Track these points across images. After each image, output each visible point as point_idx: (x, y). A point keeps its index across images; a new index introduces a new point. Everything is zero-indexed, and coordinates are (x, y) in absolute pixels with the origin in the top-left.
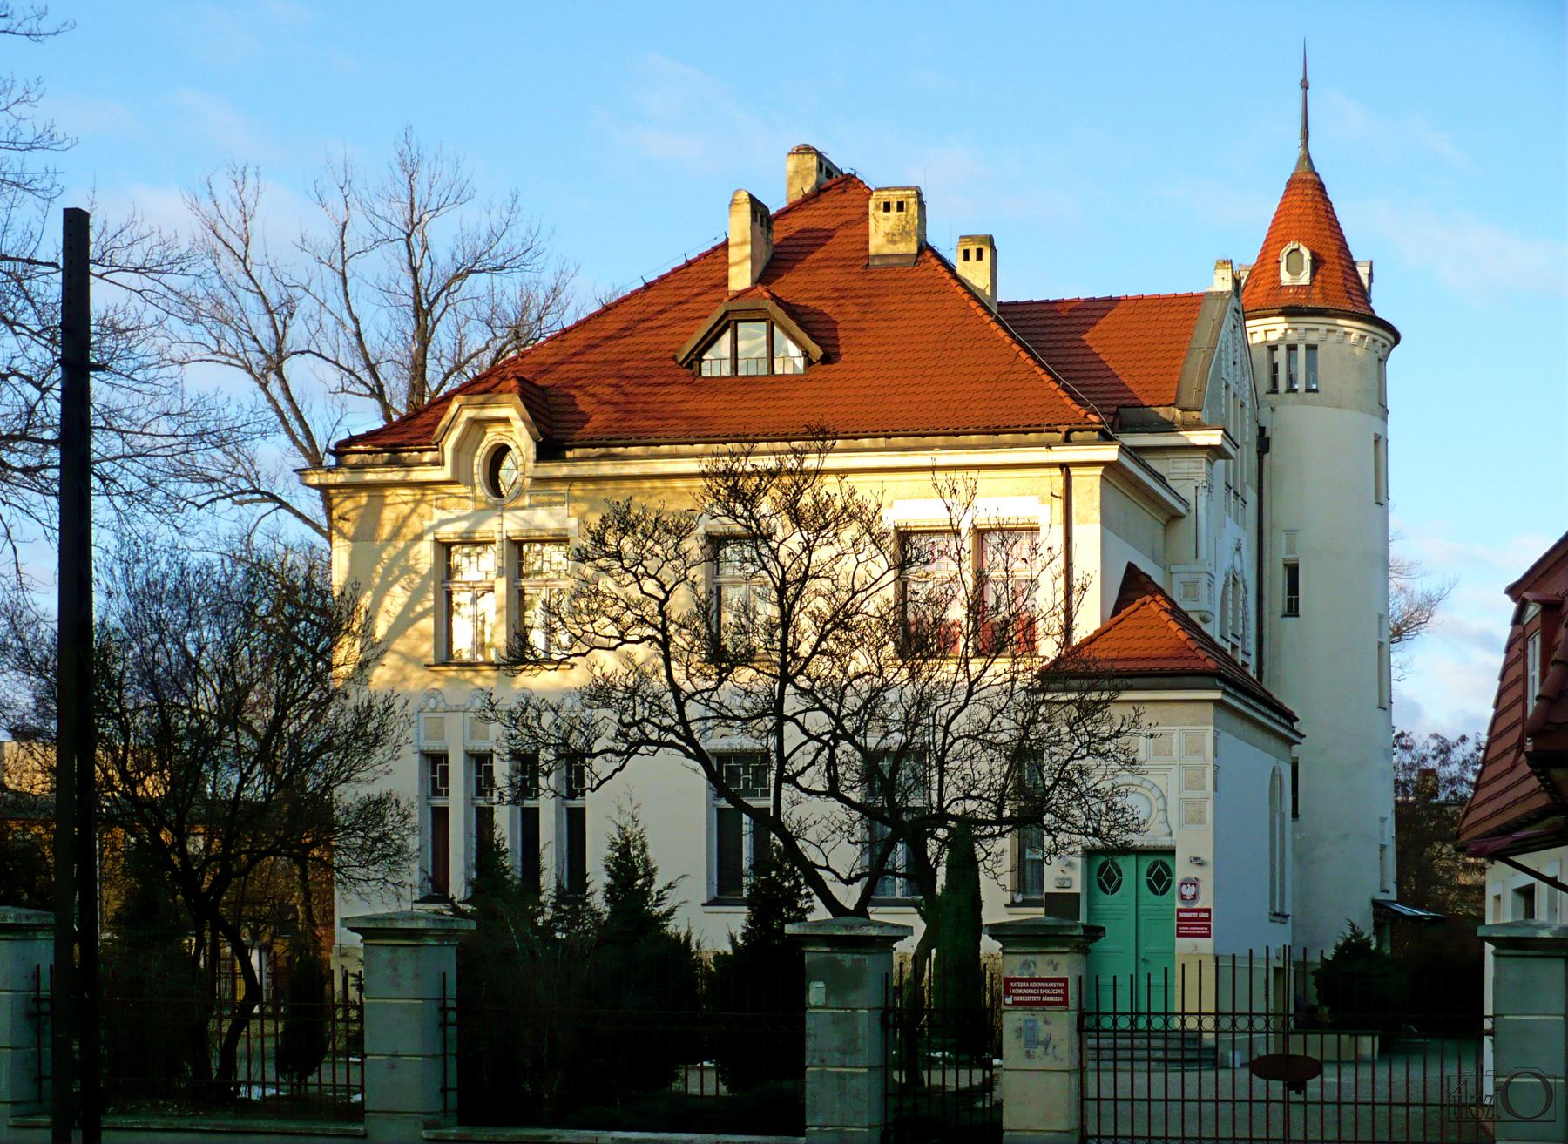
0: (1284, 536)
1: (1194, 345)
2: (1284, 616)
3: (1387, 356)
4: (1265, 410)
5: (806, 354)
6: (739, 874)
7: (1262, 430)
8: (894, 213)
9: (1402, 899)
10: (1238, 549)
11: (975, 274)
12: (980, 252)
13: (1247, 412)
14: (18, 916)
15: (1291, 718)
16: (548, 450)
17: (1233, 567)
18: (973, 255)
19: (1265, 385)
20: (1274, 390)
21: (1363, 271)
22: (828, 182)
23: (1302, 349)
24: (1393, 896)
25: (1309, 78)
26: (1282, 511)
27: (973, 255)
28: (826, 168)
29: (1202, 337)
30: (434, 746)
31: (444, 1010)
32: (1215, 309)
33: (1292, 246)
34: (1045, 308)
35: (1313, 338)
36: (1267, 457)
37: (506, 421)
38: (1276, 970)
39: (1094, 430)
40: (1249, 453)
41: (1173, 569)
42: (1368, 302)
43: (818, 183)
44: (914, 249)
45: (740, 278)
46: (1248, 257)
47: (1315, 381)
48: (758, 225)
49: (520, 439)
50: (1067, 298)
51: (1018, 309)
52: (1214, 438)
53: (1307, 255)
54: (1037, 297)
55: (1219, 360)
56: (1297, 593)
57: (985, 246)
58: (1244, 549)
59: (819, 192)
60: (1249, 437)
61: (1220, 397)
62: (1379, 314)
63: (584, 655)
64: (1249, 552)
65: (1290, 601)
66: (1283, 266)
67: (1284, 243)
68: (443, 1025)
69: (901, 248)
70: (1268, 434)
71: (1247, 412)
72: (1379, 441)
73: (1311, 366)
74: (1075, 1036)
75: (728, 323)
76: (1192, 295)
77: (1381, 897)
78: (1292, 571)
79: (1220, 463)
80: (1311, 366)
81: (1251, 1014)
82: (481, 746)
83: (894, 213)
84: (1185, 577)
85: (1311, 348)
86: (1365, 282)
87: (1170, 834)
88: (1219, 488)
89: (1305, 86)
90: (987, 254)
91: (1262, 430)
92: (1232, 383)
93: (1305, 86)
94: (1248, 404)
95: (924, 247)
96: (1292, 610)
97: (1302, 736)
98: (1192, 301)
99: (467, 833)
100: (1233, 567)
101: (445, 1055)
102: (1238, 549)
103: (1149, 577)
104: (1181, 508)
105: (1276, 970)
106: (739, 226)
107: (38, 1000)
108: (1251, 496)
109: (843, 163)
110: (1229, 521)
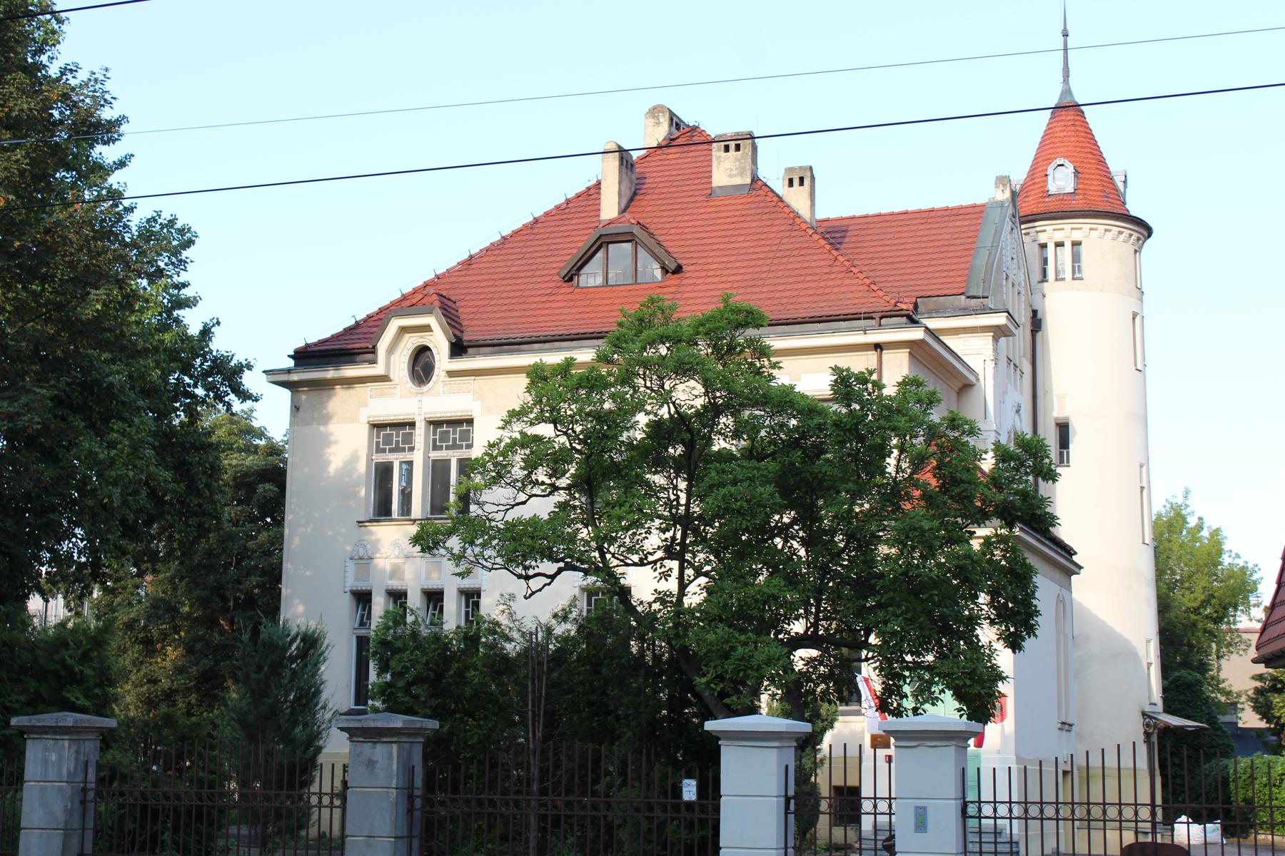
1: (979, 245)
3: (1141, 248)
4: (1038, 297)
7: (1035, 312)
8: (732, 152)
9: (1168, 709)
10: (1018, 411)
11: (797, 199)
12: (802, 180)
13: (1023, 299)
14: (76, 721)
15: (1068, 552)
16: (458, 349)
17: (1014, 426)
18: (796, 182)
19: (1036, 275)
20: (1044, 278)
21: (1118, 181)
22: (676, 133)
23: (1068, 245)
24: (1160, 707)
25: (1068, 28)
27: (796, 182)
28: (675, 122)
29: (986, 238)
30: (362, 586)
31: (411, 798)
32: (995, 215)
33: (1059, 161)
34: (876, 219)
35: (1077, 236)
36: (1039, 335)
37: (427, 328)
38: (1065, 773)
39: (902, 316)
40: (1023, 334)
42: (1124, 203)
43: (670, 133)
44: (748, 181)
45: (609, 208)
46: (1019, 175)
47: (1080, 271)
48: (624, 170)
49: (439, 342)
50: (832, 217)
51: (854, 221)
52: (1000, 319)
55: (1001, 255)
56: (1067, 447)
57: (802, 178)
58: (1022, 411)
59: (669, 143)
60: (1024, 318)
61: (1001, 286)
62: (1133, 213)
63: (524, 503)
67: (1050, 160)
68: (410, 811)
69: (738, 181)
70: (1039, 316)
71: (1023, 299)
73: (1076, 258)
74: (960, 819)
75: (603, 242)
76: (975, 206)
77: (1148, 709)
79: (1003, 340)
80: (1076, 258)
81: (1104, 804)
82: (434, 584)
83: (732, 152)
85: (1076, 244)
86: (1121, 186)
88: (1004, 361)
89: (1066, 35)
90: (807, 182)
91: (1035, 312)
92: (1011, 276)
93: (1066, 35)
95: (755, 179)
97: (1080, 568)
98: (977, 210)
100: (1014, 426)
101: (410, 837)
102: (1018, 411)
104: (973, 379)
105: (1065, 773)
106: (608, 173)
107: (84, 790)
108: (1027, 368)
109: (689, 118)
110: (1010, 388)
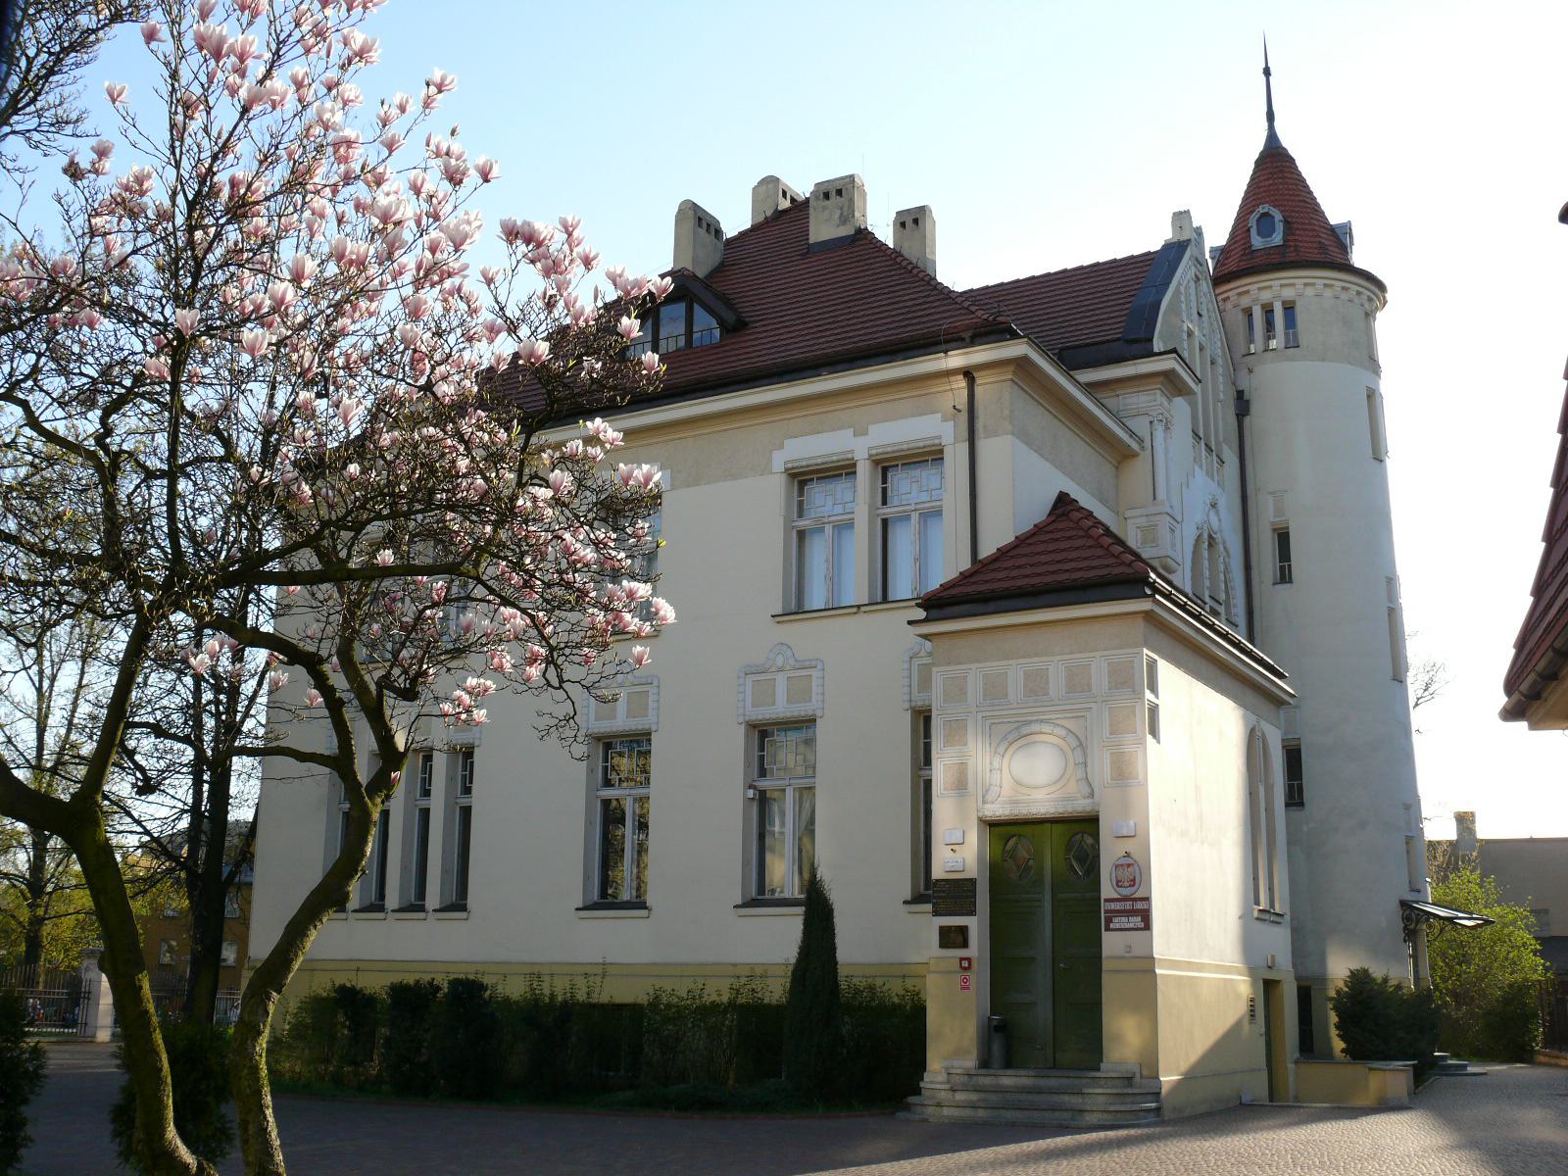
0: (1270, 499)
2: (1275, 584)
5: (722, 323)
6: (209, 844)
7: (1240, 394)
26: (1267, 473)
33: (1261, 209)
36: (1247, 420)
41: (1128, 514)
53: (1278, 216)
54: (992, 281)
64: (1229, 501)
65: (1282, 568)
66: (1254, 232)
70: (1246, 396)
71: (1220, 370)
72: (1372, 397)
78: (1283, 538)
84: (1142, 521)
87: (1092, 795)
89: (1267, 72)
91: (1240, 394)
94: (1220, 361)
96: (1285, 576)
99: (445, 871)
102: (1214, 506)
103: (1090, 514)
104: (1134, 445)
110: (1200, 474)
